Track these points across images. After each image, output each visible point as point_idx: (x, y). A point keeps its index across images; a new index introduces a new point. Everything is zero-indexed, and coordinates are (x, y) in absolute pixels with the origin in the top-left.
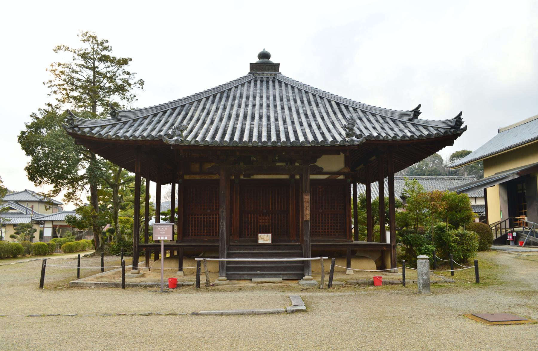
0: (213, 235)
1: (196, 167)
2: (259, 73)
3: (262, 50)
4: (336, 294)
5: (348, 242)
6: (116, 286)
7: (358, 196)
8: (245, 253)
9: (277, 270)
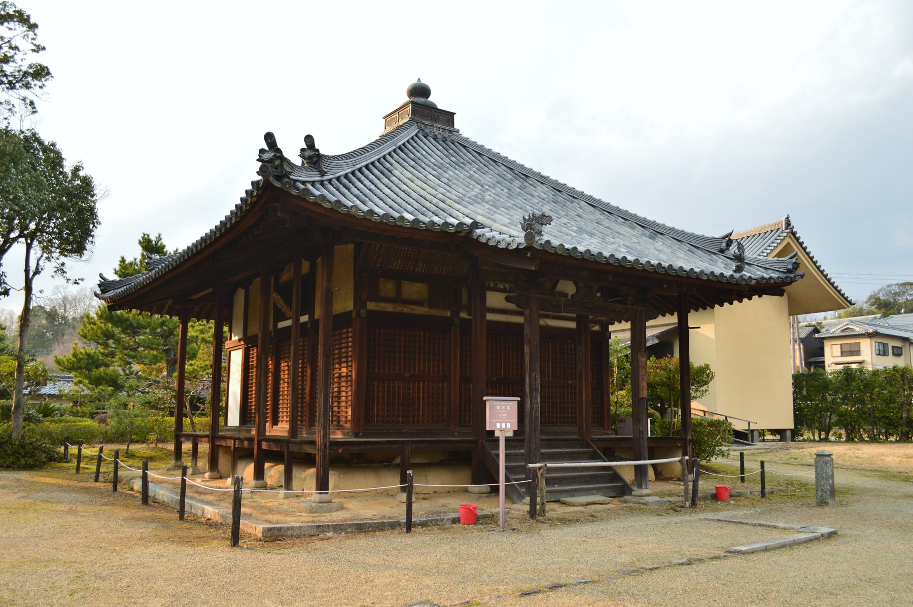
0: (413, 421)
1: (388, 288)
2: (426, 122)
3: (414, 81)
4: (687, 518)
5: (607, 434)
6: (394, 526)
7: (613, 359)
8: (517, 455)
9: (580, 483)
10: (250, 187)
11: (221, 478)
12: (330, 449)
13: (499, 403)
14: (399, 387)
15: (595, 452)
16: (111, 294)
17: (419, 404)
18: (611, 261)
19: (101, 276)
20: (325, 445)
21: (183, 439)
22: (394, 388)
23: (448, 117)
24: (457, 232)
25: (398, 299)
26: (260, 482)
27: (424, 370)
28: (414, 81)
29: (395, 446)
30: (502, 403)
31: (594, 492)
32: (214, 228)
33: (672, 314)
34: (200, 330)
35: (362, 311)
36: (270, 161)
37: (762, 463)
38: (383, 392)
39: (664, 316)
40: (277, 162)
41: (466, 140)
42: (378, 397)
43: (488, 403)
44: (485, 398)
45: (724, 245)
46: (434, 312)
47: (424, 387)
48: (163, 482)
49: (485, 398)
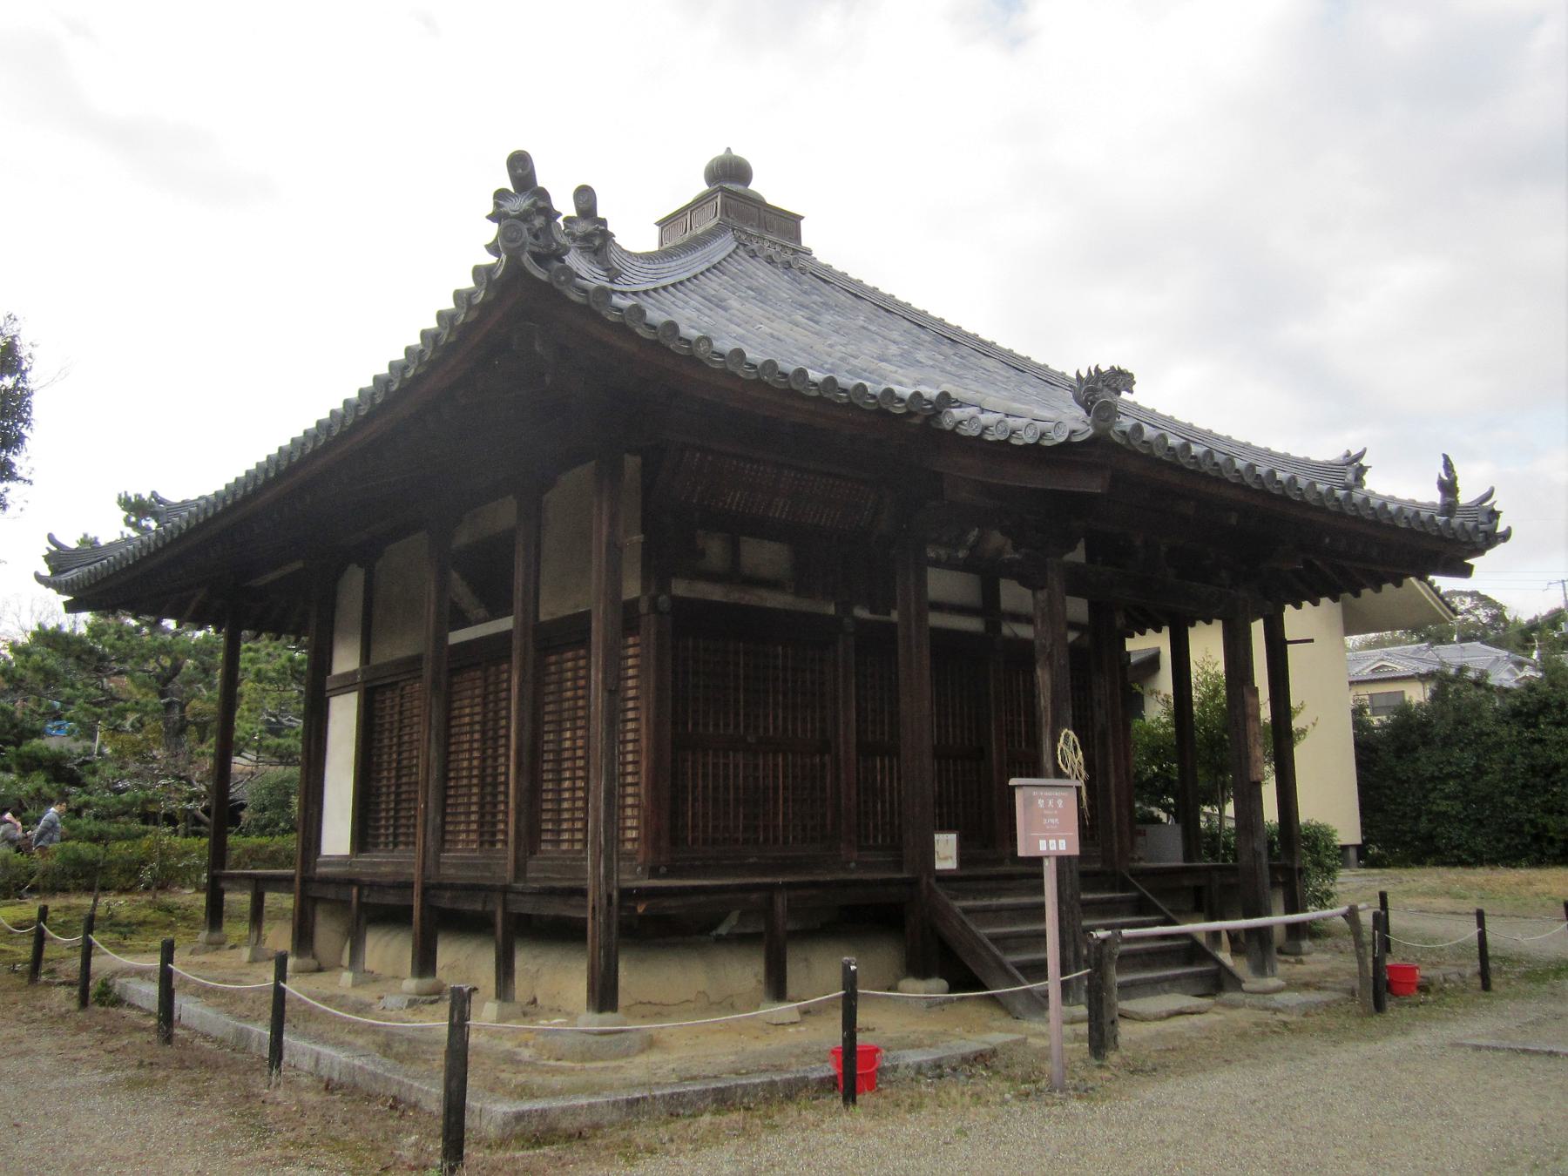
0: (766, 840)
8: (999, 909)
9: (1146, 966)
10: (449, 305)
11: (320, 970)
12: (621, 907)
13: (1042, 792)
14: (736, 766)
15: (1142, 898)
16: (73, 574)
17: (776, 802)
18: (1249, 480)
19: (51, 538)
20: (610, 897)
21: (224, 885)
22: (726, 765)
23: (788, 224)
24: (910, 414)
25: (734, 575)
26: (428, 982)
27: (785, 730)
28: (720, 152)
29: (754, 896)
30: (1048, 793)
31: (1166, 986)
32: (401, 356)
33: (1158, 630)
34: (269, 655)
35: (663, 598)
36: (524, 217)
37: (1480, 916)
38: (705, 775)
39: (1143, 633)
40: (539, 222)
41: (828, 268)
42: (695, 787)
43: (1019, 794)
44: (1013, 782)
45: (1350, 477)
46: (805, 605)
47: (785, 766)
48: (130, 967)
49: (1013, 782)
